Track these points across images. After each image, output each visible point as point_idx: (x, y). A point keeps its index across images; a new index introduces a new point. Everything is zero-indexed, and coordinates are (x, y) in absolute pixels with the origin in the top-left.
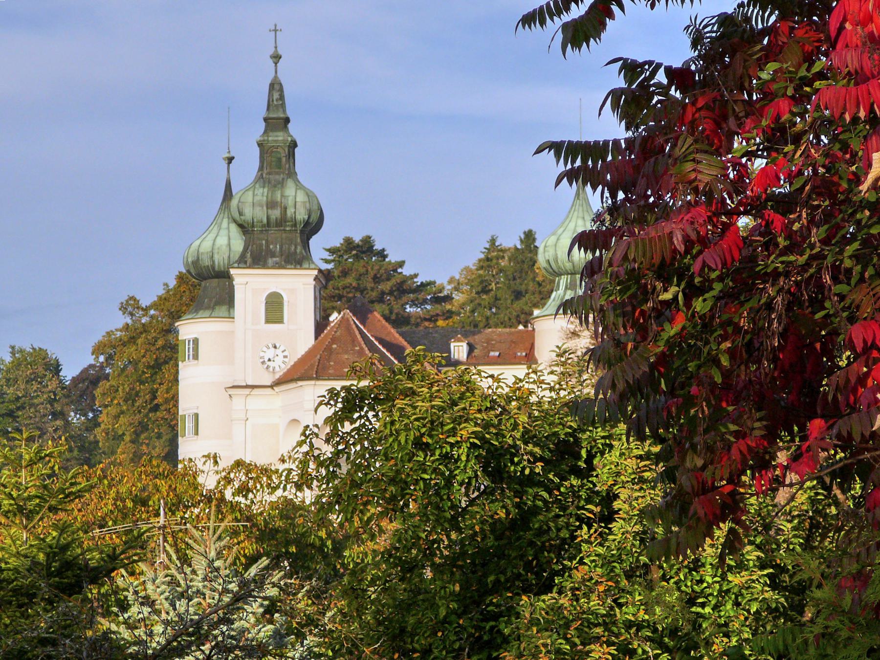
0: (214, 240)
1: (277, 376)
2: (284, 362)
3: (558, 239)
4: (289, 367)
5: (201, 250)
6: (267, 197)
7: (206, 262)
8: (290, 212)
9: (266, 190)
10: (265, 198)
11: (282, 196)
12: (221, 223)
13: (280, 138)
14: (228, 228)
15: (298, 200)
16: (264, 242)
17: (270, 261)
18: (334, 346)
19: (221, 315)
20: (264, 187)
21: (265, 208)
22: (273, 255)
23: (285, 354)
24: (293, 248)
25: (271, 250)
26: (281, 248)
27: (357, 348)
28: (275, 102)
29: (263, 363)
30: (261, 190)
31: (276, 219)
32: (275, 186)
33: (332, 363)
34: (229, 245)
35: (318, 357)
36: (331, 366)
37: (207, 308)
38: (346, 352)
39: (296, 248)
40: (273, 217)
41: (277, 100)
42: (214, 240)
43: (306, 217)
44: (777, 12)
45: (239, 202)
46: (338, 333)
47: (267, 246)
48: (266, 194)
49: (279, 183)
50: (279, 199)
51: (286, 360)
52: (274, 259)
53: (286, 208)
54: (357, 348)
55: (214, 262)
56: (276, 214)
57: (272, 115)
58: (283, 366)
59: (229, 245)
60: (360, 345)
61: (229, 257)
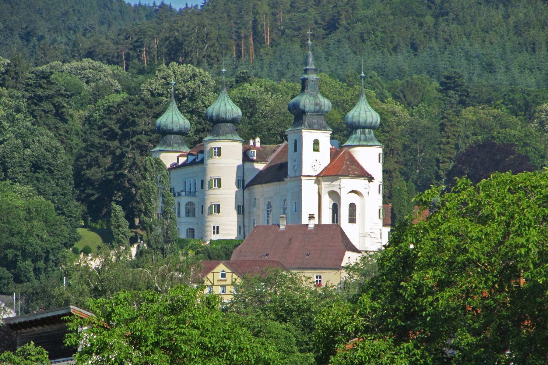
8: (323, 107)
17: (315, 127)
22: (315, 124)
56: (318, 108)
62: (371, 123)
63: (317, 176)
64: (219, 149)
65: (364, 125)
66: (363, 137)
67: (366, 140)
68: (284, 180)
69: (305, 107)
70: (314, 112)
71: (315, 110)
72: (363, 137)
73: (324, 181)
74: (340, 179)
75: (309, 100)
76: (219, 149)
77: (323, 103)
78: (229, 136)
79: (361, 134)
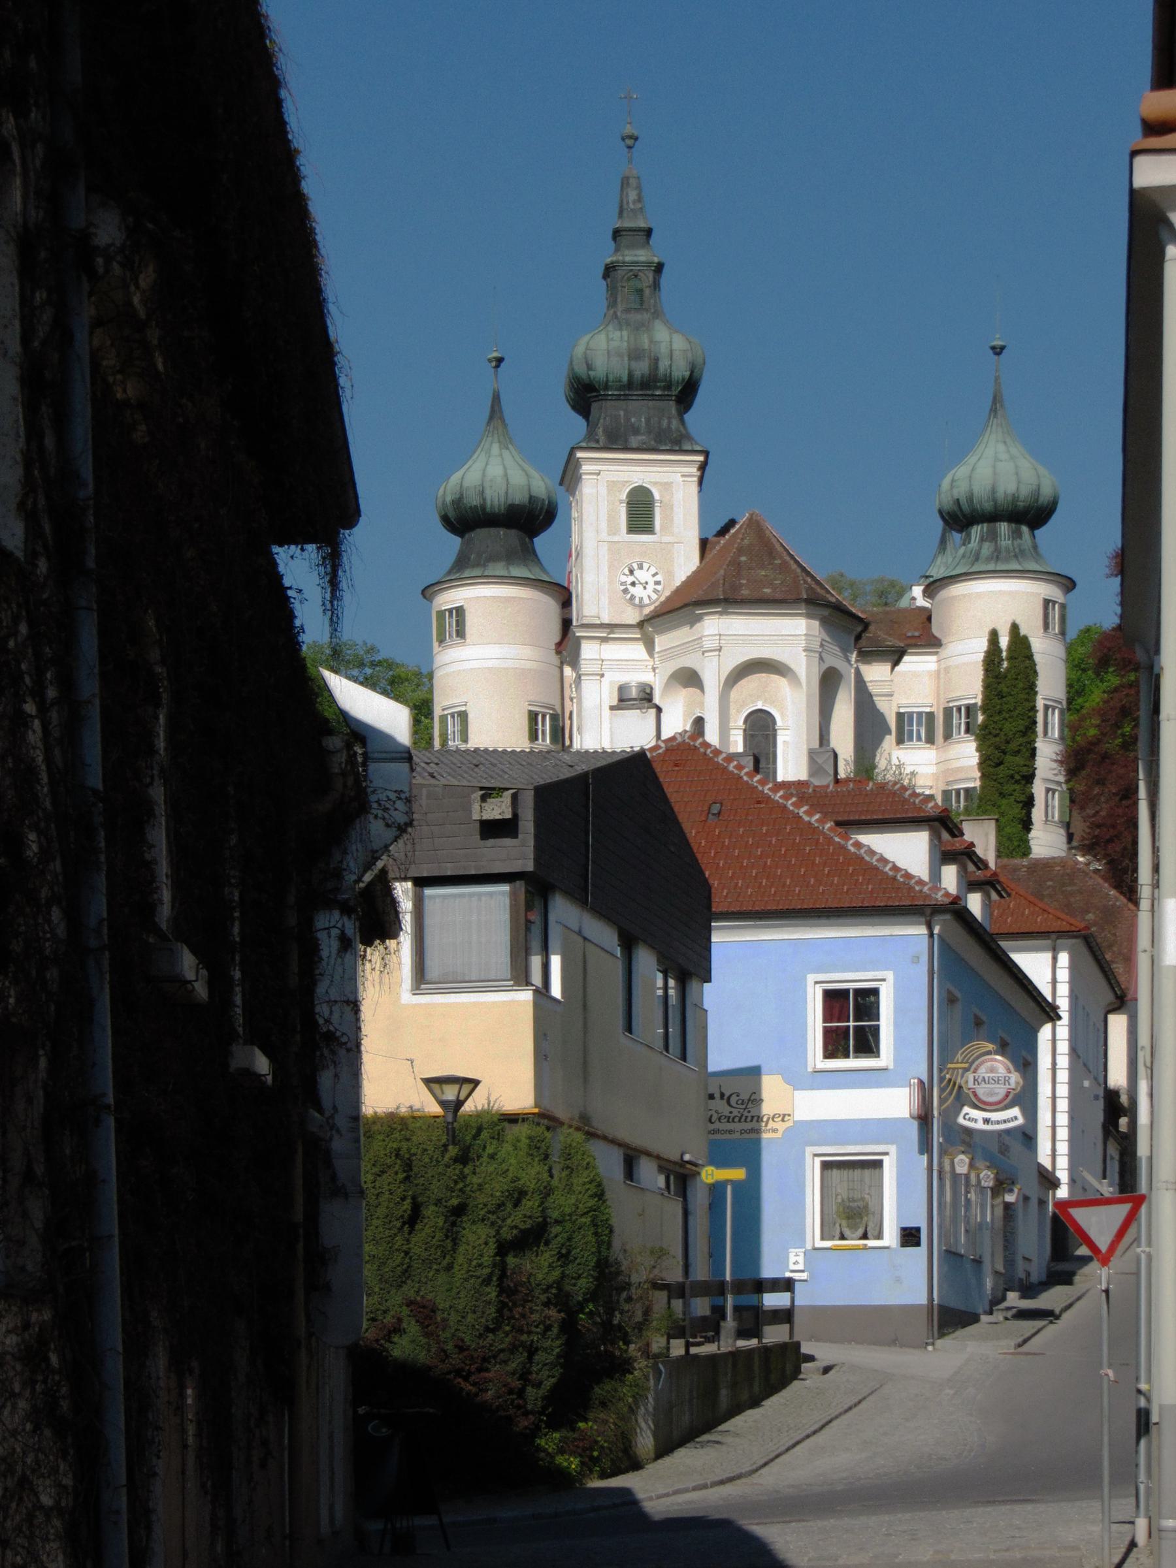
0: (484, 470)
1: (647, 611)
2: (655, 591)
3: (973, 469)
4: (663, 599)
5: (466, 484)
6: (628, 342)
7: (473, 500)
8: (663, 365)
9: (625, 333)
10: (625, 344)
11: (651, 341)
12: (490, 449)
13: (643, 259)
14: (501, 455)
15: (675, 346)
16: (622, 413)
17: (634, 441)
18: (743, 559)
19: (497, 573)
20: (621, 329)
21: (626, 359)
22: (636, 431)
23: (658, 578)
24: (665, 423)
25: (632, 425)
26: (648, 421)
27: (778, 562)
28: (632, 206)
29: (626, 591)
30: (618, 333)
31: (643, 376)
32: (637, 329)
33: (744, 582)
34: (506, 475)
35: (722, 572)
36: (743, 585)
37: (477, 565)
38: (762, 567)
39: (669, 423)
40: (637, 374)
41: (634, 202)
42: (484, 470)
43: (687, 374)
44: (237, 939)
45: (587, 349)
46: (746, 542)
47: (628, 419)
48: (626, 338)
49: (643, 325)
50: (646, 347)
51: (659, 588)
52: (640, 438)
53: (657, 360)
54: (778, 562)
55: (484, 499)
56: (642, 368)
57: (628, 224)
58: (654, 597)
59: (506, 475)
60: (781, 558)
61: (507, 493)
62: (1015, 498)
63: (641, 625)
64: (460, 612)
65: (988, 506)
66: (987, 548)
67: (997, 556)
68: (283, 575)
69: (589, 367)
70: (630, 385)
71: (630, 375)
72: (987, 548)
73: (660, 632)
74: (699, 618)
75: (609, 340)
76: (460, 612)
77: (664, 349)
78: (499, 569)
79: (982, 540)
